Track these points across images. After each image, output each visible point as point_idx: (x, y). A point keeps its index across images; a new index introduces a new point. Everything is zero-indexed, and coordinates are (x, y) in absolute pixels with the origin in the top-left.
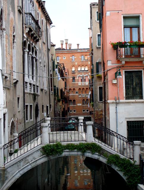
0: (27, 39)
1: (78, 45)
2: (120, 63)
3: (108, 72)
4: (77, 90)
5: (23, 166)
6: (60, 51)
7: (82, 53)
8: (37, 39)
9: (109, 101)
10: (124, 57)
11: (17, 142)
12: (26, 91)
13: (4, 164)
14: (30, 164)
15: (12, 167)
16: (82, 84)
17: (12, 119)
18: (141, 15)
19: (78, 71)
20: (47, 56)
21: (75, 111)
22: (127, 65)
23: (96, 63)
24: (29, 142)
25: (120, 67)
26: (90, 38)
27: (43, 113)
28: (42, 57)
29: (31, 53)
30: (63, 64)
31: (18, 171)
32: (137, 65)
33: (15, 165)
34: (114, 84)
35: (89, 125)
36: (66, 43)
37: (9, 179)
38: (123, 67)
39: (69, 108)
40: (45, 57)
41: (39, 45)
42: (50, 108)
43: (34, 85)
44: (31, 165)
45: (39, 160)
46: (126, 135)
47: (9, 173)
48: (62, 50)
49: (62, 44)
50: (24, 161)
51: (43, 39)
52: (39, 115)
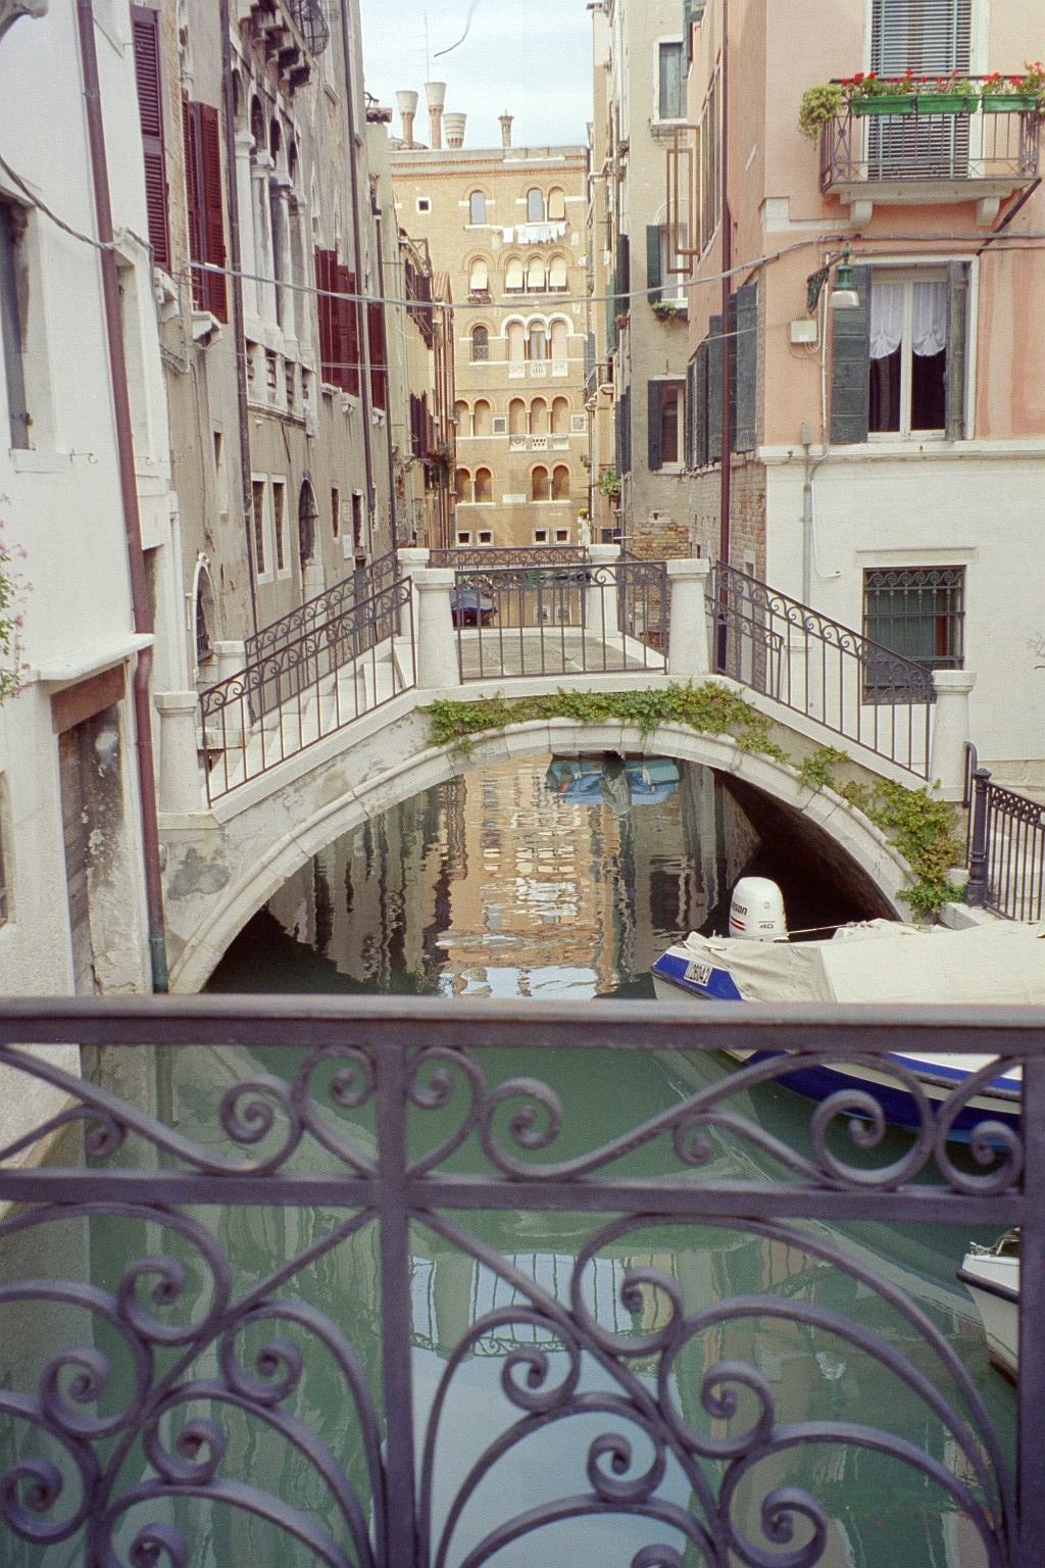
0: (246, 65)
1: (506, 121)
3: (769, 270)
8: (301, 63)
9: (764, 452)
10: (864, 173)
11: (240, 696)
13: (210, 801)
17: (201, 556)
19: (509, 290)
20: (349, 183)
22: (883, 229)
23: (649, 228)
26: (596, 68)
27: (336, 535)
28: (324, 189)
29: (264, 156)
31: (287, 838)
32: (940, 227)
33: (270, 803)
34: (802, 345)
35: (685, 578)
36: (437, 111)
37: (244, 879)
38: (858, 238)
40: (336, 187)
41: (307, 110)
42: (371, 507)
43: (288, 364)
44: (363, 804)
45: (406, 778)
46: (416, 1352)
47: (237, 847)
50: (320, 781)
51: (321, 73)
52: (317, 548)
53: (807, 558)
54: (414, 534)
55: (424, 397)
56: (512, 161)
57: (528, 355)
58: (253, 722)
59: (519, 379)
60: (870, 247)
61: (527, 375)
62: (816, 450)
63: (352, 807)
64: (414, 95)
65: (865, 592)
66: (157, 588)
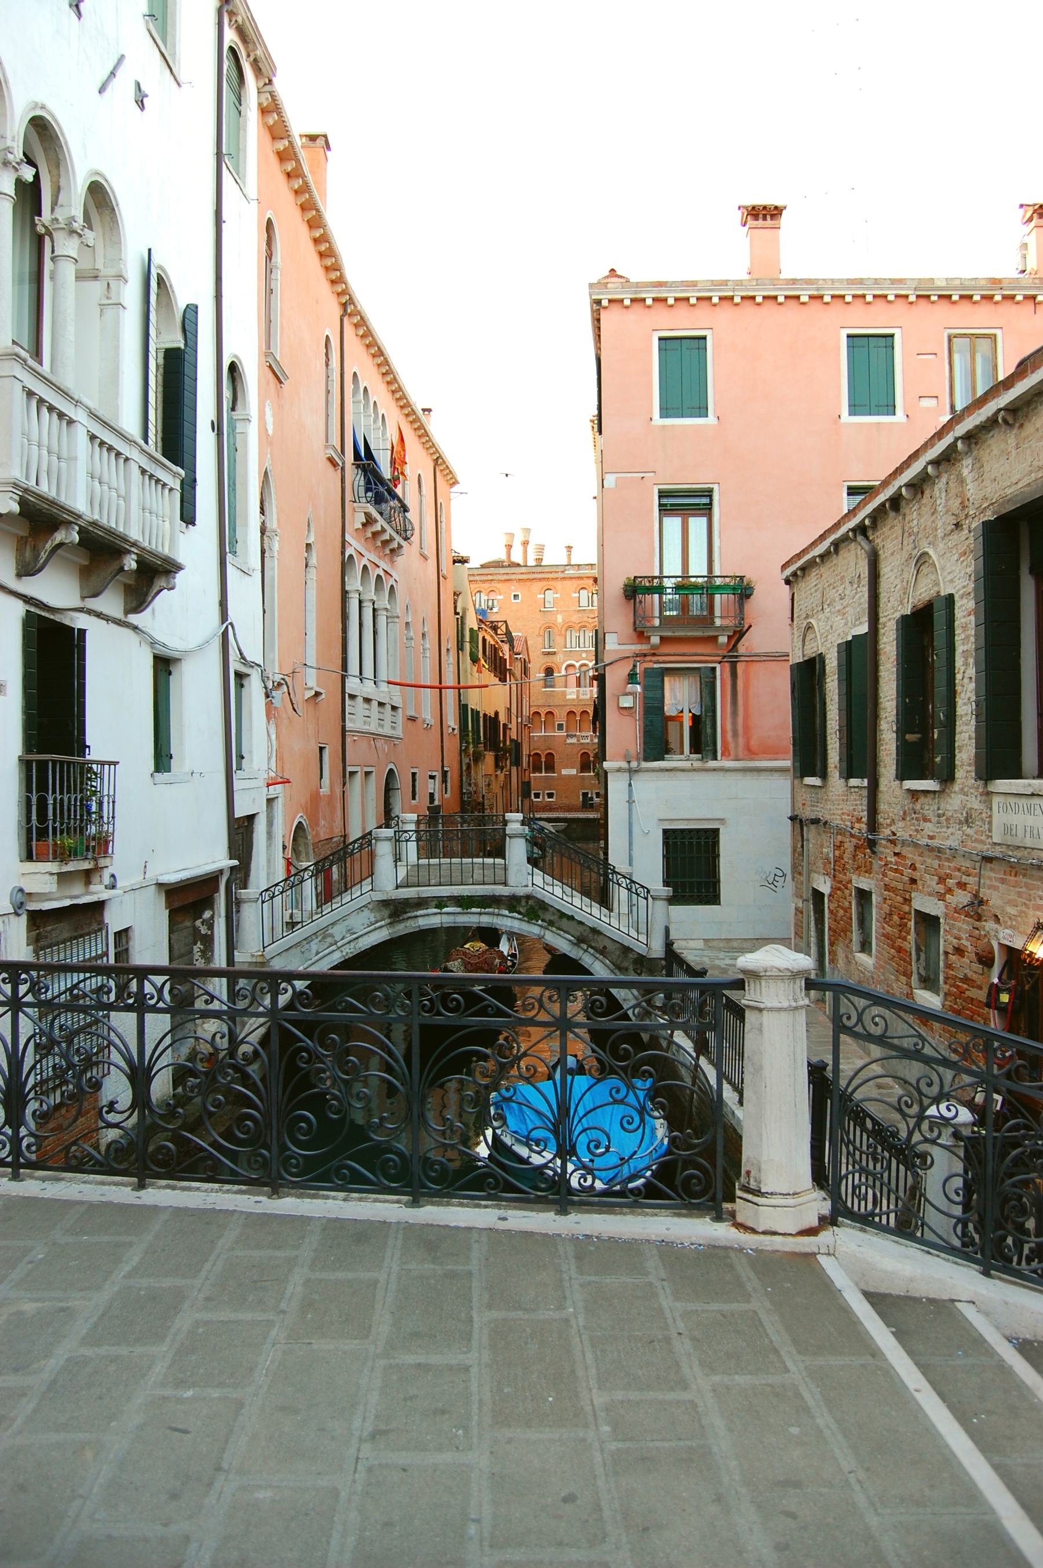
1: (569, 548)
2: (644, 641)
4: (561, 717)
5: (317, 953)
6: (502, 570)
7: (580, 578)
12: (351, 725)
13: (264, 948)
14: (339, 948)
15: (285, 953)
16: (581, 697)
18: (716, 487)
21: (550, 795)
22: (667, 649)
24: (355, 885)
25: (645, 655)
30: (505, 622)
34: (626, 708)
36: (525, 544)
38: (654, 655)
39: (529, 783)
44: (342, 952)
45: (366, 937)
48: (509, 566)
49: (509, 547)
53: (630, 824)
54: (483, 796)
55: (497, 714)
56: (571, 572)
57: (579, 685)
58: (318, 908)
59: (573, 700)
60: (661, 659)
61: (578, 697)
62: (634, 764)
63: (336, 952)
64: (512, 535)
65: (664, 842)
66: (255, 835)
